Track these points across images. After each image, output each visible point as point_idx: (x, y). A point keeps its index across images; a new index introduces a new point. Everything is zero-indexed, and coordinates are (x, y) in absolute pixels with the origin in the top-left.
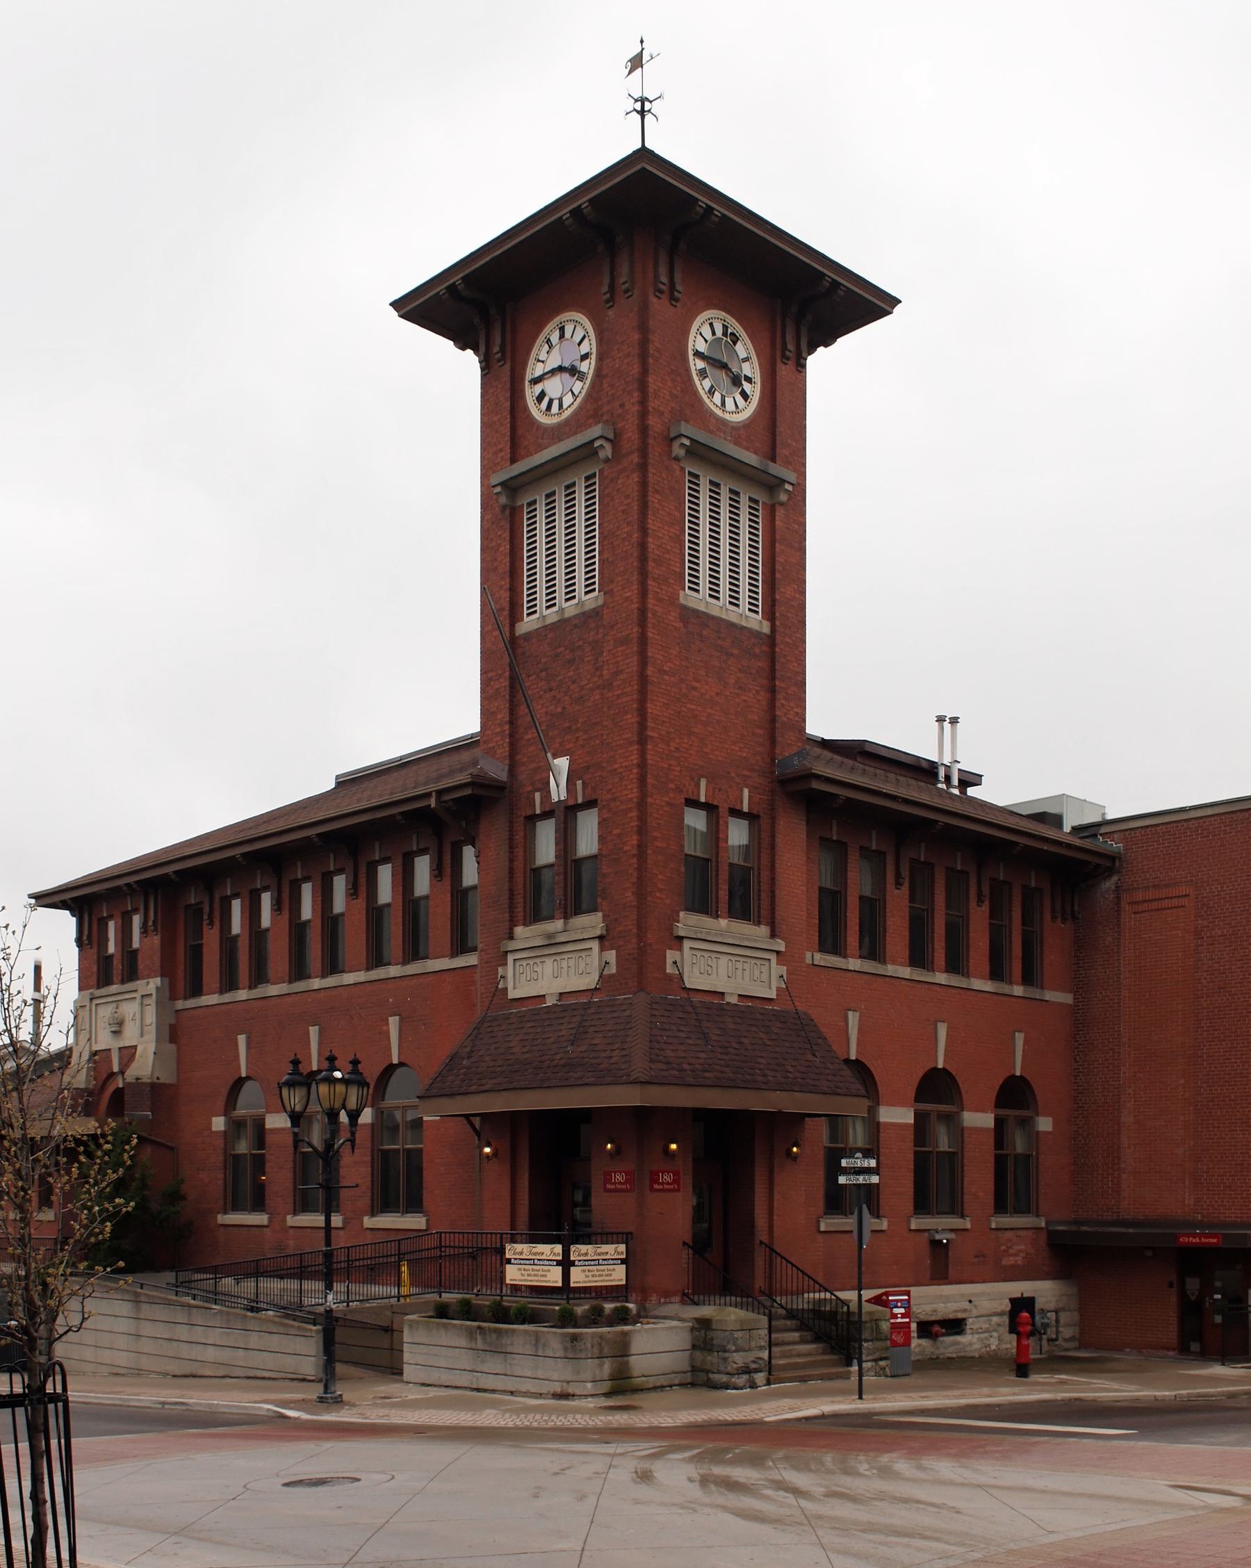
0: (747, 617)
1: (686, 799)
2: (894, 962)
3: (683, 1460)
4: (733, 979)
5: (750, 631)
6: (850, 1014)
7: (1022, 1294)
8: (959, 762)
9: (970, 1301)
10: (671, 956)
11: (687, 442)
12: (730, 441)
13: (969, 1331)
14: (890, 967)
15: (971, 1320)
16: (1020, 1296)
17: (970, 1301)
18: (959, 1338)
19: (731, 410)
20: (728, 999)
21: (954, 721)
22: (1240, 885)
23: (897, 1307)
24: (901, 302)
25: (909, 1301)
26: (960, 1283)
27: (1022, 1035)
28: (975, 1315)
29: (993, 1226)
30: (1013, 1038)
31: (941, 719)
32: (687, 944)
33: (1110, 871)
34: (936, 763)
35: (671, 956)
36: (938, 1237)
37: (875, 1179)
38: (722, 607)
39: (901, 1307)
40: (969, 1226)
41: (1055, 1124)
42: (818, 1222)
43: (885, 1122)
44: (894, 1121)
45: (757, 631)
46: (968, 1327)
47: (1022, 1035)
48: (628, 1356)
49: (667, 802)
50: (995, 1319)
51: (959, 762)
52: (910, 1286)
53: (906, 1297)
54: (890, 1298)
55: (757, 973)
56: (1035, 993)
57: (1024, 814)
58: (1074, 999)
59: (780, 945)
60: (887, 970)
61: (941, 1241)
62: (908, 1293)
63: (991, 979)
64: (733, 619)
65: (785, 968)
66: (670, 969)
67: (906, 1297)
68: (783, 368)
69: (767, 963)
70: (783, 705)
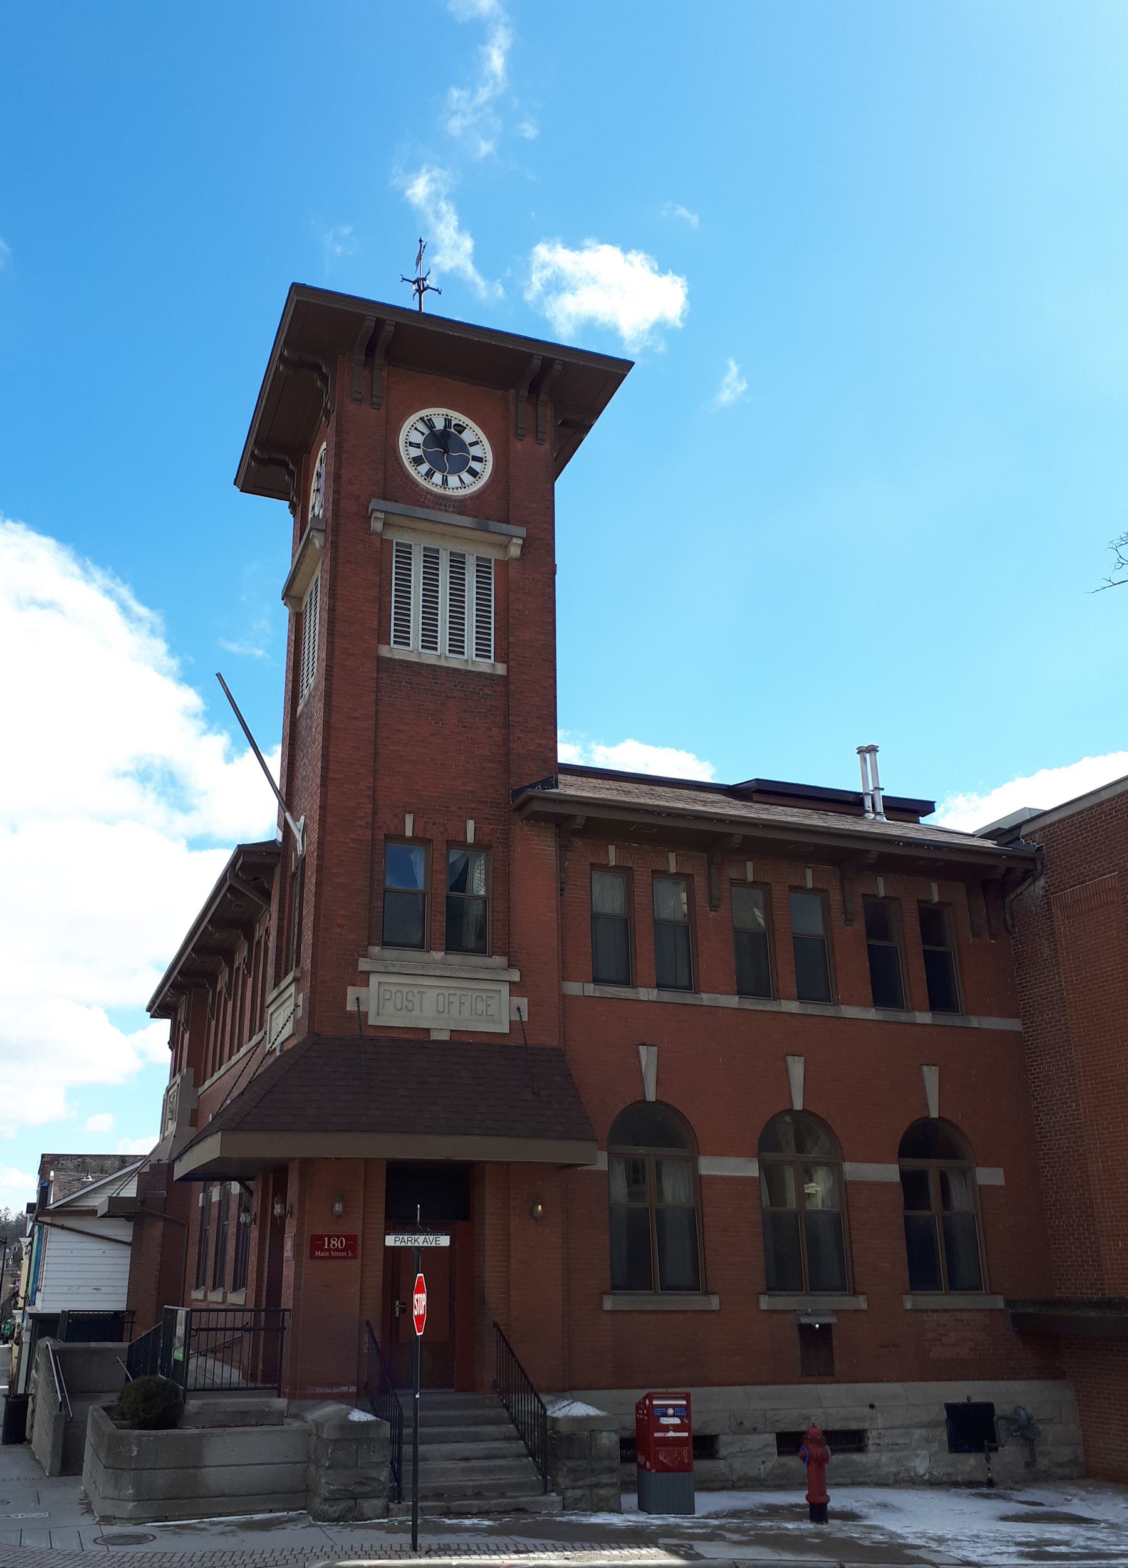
0: (473, 662)
1: (790, 886)
2: (712, 990)
3: (703, 1558)
4: (445, 1015)
5: (481, 675)
6: (642, 1049)
7: (969, 1398)
8: (883, 789)
9: (872, 1406)
10: (352, 992)
11: (382, 516)
12: (453, 512)
13: (871, 1448)
14: (704, 996)
15: (874, 1433)
16: (965, 1400)
17: (872, 1406)
18: (856, 1457)
19: (454, 486)
20: (435, 1036)
21: (872, 750)
22: (1116, 856)
23: (666, 1415)
24: (632, 364)
25: (687, 1408)
26: (856, 1382)
27: (935, 1070)
28: (880, 1426)
29: (908, 1306)
30: (920, 1075)
31: (861, 751)
32: (374, 980)
33: (1029, 875)
34: (861, 794)
35: (352, 992)
36: (805, 1320)
37: (326, 1247)
38: (467, 661)
39: (674, 1416)
40: (864, 1306)
41: (1008, 1177)
42: (601, 1299)
43: (709, 1176)
44: (725, 1174)
45: (490, 674)
46: (870, 1442)
47: (935, 1070)
48: (200, 1467)
49: (354, 839)
50: (918, 1433)
51: (883, 789)
52: (692, 1386)
53: (684, 1402)
54: (655, 1402)
55: (481, 1006)
56: (955, 1021)
57: (971, 832)
58: (1024, 1024)
59: (515, 976)
60: (701, 999)
61: (811, 1326)
62: (687, 1397)
63: (931, 1010)
64: (432, 661)
65: (526, 999)
66: (351, 1007)
67: (684, 1402)
68: (519, 444)
69: (496, 995)
70: (519, 738)
